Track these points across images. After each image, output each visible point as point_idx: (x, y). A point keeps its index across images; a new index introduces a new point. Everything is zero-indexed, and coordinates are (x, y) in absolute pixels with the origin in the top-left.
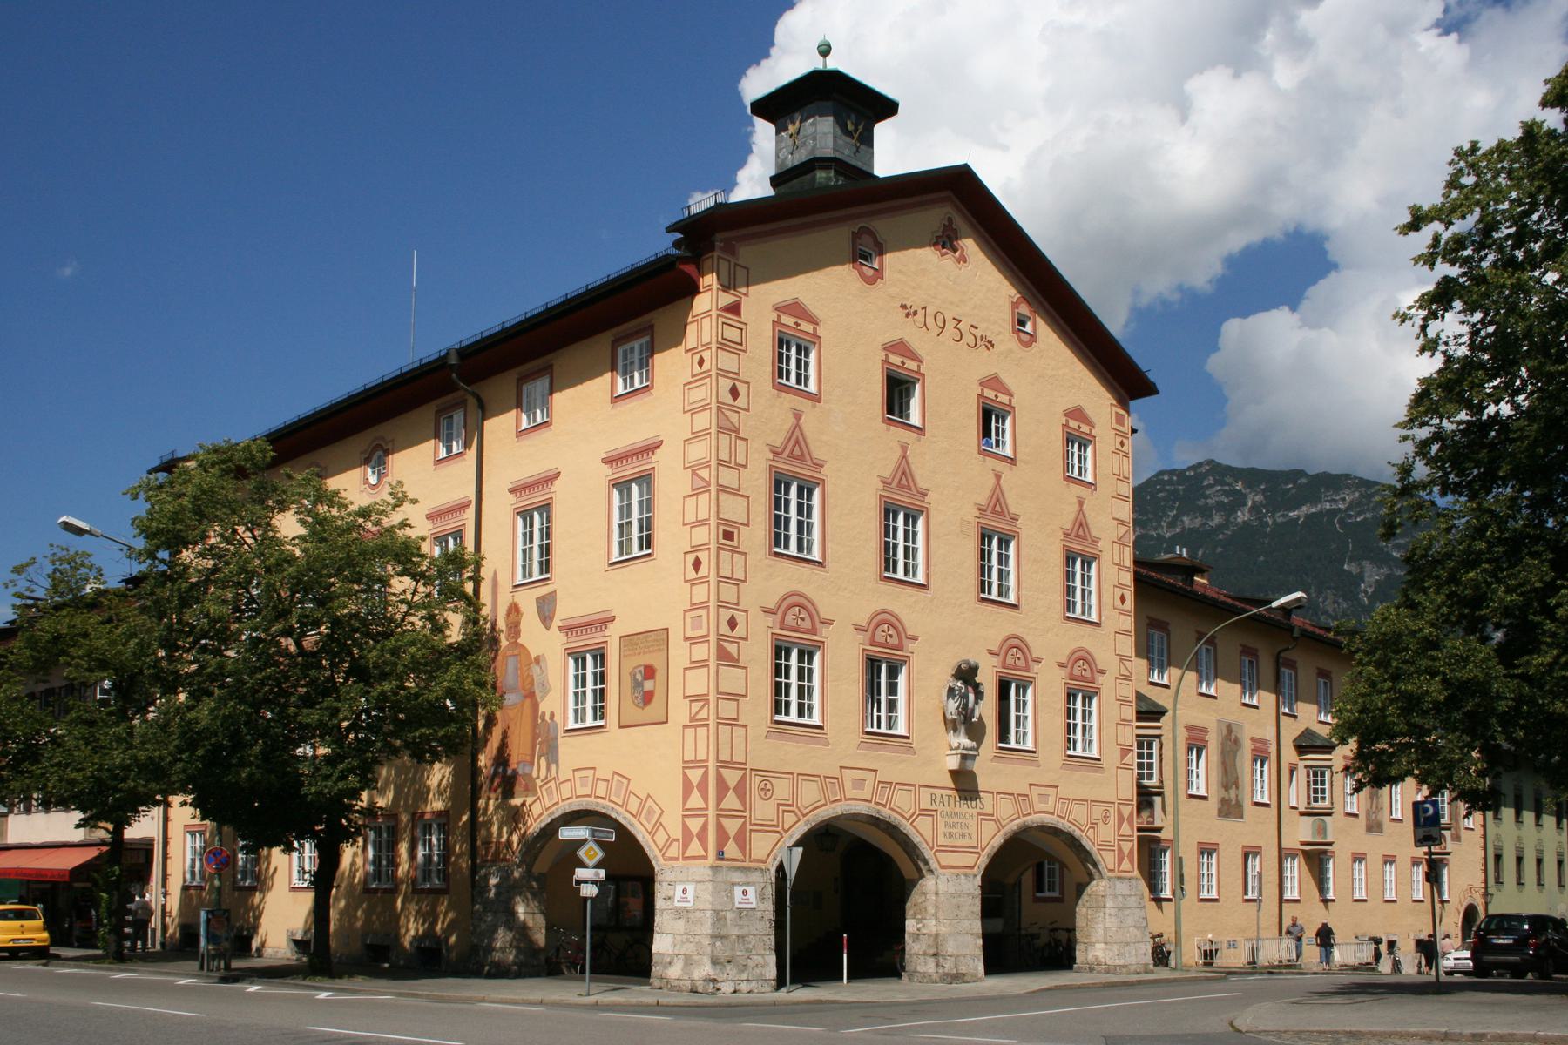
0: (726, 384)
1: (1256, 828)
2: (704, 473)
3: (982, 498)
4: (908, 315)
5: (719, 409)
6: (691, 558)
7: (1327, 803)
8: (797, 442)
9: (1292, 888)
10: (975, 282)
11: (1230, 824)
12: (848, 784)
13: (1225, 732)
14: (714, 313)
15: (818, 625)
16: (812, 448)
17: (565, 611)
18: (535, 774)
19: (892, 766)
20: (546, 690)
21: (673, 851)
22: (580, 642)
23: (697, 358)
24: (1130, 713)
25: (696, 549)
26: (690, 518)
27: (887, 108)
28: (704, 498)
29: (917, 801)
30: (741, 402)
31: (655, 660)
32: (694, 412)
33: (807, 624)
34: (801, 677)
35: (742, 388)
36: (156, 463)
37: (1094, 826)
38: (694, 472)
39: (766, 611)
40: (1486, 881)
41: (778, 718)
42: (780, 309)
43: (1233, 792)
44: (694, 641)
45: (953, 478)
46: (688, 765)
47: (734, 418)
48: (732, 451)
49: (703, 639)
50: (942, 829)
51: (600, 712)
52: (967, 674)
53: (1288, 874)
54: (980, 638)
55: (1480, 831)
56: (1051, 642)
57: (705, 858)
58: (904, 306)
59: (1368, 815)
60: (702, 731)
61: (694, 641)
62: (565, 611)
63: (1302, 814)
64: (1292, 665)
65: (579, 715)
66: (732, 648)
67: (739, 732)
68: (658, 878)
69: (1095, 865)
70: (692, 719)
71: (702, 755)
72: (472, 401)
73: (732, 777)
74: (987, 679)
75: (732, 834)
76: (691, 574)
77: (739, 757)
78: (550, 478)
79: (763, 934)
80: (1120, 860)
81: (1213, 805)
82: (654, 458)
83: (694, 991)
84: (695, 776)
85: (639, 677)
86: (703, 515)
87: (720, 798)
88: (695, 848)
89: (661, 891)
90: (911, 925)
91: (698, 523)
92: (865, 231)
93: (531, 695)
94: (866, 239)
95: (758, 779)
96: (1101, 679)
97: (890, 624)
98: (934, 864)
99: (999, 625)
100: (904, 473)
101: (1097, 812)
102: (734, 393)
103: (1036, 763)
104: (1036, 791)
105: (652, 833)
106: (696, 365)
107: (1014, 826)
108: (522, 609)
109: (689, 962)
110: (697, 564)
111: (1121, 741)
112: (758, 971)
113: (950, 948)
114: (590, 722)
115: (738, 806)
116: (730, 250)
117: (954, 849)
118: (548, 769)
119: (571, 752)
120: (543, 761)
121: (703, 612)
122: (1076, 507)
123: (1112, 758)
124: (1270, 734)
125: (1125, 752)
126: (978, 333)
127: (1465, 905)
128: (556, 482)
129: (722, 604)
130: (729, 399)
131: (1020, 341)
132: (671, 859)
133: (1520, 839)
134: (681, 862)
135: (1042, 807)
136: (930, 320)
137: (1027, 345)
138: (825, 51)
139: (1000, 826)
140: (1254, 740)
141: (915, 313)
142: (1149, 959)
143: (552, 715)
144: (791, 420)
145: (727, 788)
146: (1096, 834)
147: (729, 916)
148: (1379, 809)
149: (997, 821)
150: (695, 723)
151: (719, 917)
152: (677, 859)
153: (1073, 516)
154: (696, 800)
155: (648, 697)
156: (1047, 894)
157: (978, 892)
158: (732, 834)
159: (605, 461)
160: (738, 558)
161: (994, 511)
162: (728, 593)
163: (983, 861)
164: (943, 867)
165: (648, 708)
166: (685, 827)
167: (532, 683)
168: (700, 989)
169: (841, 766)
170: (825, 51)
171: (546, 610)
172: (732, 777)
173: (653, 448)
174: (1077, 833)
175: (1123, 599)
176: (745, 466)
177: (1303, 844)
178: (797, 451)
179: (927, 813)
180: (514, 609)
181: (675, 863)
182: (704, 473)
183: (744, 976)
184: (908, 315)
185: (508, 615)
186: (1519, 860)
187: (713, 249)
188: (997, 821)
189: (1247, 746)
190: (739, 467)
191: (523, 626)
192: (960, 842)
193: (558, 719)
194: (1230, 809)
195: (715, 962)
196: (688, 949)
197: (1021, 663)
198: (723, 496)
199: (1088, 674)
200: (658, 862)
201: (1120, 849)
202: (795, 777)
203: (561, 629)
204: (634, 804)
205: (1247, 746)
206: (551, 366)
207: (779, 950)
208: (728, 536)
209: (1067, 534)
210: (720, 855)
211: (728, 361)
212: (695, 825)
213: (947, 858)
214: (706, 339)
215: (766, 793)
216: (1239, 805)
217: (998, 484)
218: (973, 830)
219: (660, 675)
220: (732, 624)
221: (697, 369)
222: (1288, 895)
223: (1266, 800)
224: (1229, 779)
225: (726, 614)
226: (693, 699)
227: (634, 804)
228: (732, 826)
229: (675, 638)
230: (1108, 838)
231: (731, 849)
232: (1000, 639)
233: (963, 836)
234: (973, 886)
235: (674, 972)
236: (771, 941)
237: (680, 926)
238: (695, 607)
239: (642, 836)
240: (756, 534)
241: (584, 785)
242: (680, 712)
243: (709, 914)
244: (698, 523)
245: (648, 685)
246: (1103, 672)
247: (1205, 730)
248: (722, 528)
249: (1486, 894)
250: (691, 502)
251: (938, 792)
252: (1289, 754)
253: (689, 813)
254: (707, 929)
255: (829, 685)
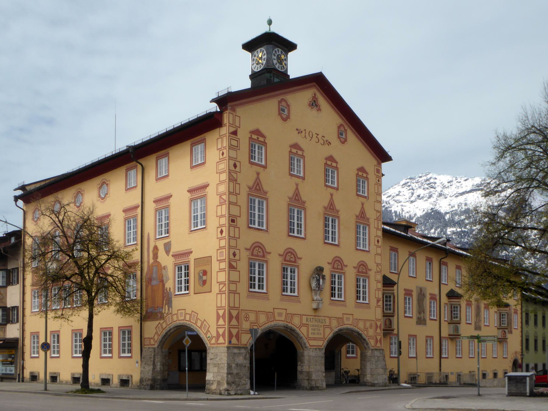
0: (232, 163)
1: (431, 328)
2: (224, 197)
3: (326, 204)
4: (299, 133)
5: (229, 172)
6: (219, 230)
7: (458, 319)
8: (258, 184)
9: (445, 353)
10: (329, 118)
11: (421, 327)
12: (276, 315)
13: (419, 291)
14: (227, 135)
15: (265, 254)
16: (263, 186)
17: (175, 249)
18: (164, 312)
19: (293, 308)
20: (168, 279)
21: (213, 341)
22: (180, 261)
23: (221, 152)
24: (380, 285)
25: (221, 226)
26: (219, 214)
27: (291, 46)
28: (224, 207)
29: (301, 320)
30: (238, 169)
31: (206, 268)
32: (220, 173)
33: (261, 254)
34: (259, 274)
35: (238, 164)
36: (17, 187)
37: (366, 329)
38: (220, 197)
39: (246, 249)
40: (522, 350)
41: (251, 290)
42: (252, 132)
43: (422, 315)
44: (220, 261)
45: (316, 198)
46: (218, 308)
47: (235, 175)
48: (234, 188)
49: (224, 261)
50: (310, 331)
51: (187, 288)
52: (319, 271)
53: (443, 347)
54: (323, 257)
55: (520, 329)
56: (351, 259)
57: (224, 343)
58: (297, 130)
59: (475, 323)
60: (223, 296)
61: (220, 261)
62: (175, 249)
63: (449, 323)
64: (446, 264)
65: (180, 289)
66: (234, 264)
67: (237, 296)
68: (208, 351)
69: (367, 344)
70: (220, 291)
71: (223, 305)
72: (139, 167)
73: (234, 313)
74: (327, 272)
75: (234, 334)
76: (219, 236)
77: (237, 305)
78: (169, 197)
79: (246, 372)
80: (376, 343)
81: (415, 319)
82: (206, 191)
83: (221, 394)
84: (221, 312)
85: (201, 275)
86: (224, 213)
87: (230, 321)
88: (221, 340)
89: (209, 356)
90: (299, 368)
91: (222, 216)
92: (283, 100)
93: (162, 281)
94: (284, 104)
95: (244, 313)
96: (370, 273)
97: (292, 253)
98: (308, 345)
99: (330, 253)
100: (297, 195)
101: (368, 324)
102: (235, 166)
103: (345, 306)
104: (345, 316)
105: (206, 334)
106: (221, 155)
107: (336, 330)
108: (159, 248)
109: (219, 383)
110: (222, 232)
111: (377, 296)
112: (243, 386)
113: (314, 377)
114: (183, 292)
115: (237, 324)
116: (234, 110)
117: (315, 339)
118: (169, 310)
119: (178, 303)
120: (167, 306)
121: (224, 250)
122: (361, 206)
123: (374, 302)
124: (436, 292)
125: (378, 301)
126: (325, 139)
127: (514, 359)
128: (171, 199)
129: (230, 247)
130: (233, 168)
131: (340, 141)
132: (213, 344)
133: (536, 332)
134: (216, 345)
135: (348, 323)
136: (307, 134)
137: (343, 143)
138: (270, 22)
139: (245, 348)
140: (430, 294)
141: (302, 132)
142: (387, 381)
143: (170, 289)
144: (255, 176)
145: (233, 317)
146: (367, 333)
147: (233, 365)
148: (480, 321)
149: (331, 328)
150: (221, 292)
151: (229, 367)
152: (214, 344)
153: (360, 209)
154: (221, 322)
155: (204, 282)
156: (351, 355)
157: (324, 355)
158: (234, 334)
159: (189, 191)
160: (237, 230)
161: (330, 208)
162: (233, 243)
163: (326, 343)
164: (310, 346)
165: (205, 287)
166: (217, 332)
167: (162, 277)
168: (223, 393)
169: (273, 310)
170: (270, 22)
171: (168, 247)
172: (234, 313)
173: (205, 186)
174: (360, 332)
175: (378, 241)
176: (239, 194)
177: (449, 335)
178: (258, 188)
179: (306, 325)
180: (156, 248)
181: (214, 346)
182: (224, 197)
183: (239, 388)
184: (299, 133)
185: (154, 250)
186: (536, 341)
187: (227, 110)
188: (331, 328)
189: (428, 297)
190: (236, 194)
191: (159, 255)
192: (316, 336)
193: (172, 290)
194: (421, 321)
195: (228, 383)
196: (219, 378)
197: (340, 267)
198: (231, 206)
199: (364, 271)
200: (208, 345)
201: (376, 338)
202: (257, 313)
203: (173, 256)
204: (199, 324)
205: (428, 297)
206: (168, 153)
207: (251, 379)
208: (233, 221)
209: (357, 216)
210: (230, 342)
211: (233, 154)
212: (221, 331)
213: (312, 343)
214: (225, 145)
215: (247, 318)
216: (425, 320)
217: (332, 198)
218: (322, 332)
219: (209, 274)
220: (234, 255)
221: (221, 157)
222: (443, 356)
223: (435, 318)
224: (421, 310)
225: (232, 251)
226: (220, 283)
227: (199, 324)
228: (234, 332)
229: (214, 260)
230: (372, 335)
231: (234, 341)
232: (332, 258)
233: (318, 334)
234: (322, 353)
235: (214, 387)
236: (248, 374)
237: (216, 369)
238: (221, 248)
239: (202, 336)
240: (242, 222)
241: (181, 316)
242: (215, 288)
243: (226, 365)
244: (222, 216)
245: (204, 278)
246: (370, 270)
247: (412, 291)
248: (230, 218)
249: (522, 355)
250: (219, 208)
251: (309, 317)
252: (444, 299)
253: (218, 327)
254: (225, 371)
255: (308, 221)
